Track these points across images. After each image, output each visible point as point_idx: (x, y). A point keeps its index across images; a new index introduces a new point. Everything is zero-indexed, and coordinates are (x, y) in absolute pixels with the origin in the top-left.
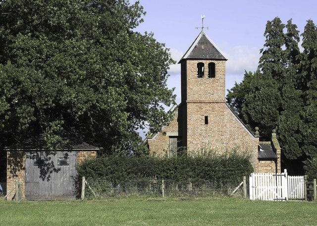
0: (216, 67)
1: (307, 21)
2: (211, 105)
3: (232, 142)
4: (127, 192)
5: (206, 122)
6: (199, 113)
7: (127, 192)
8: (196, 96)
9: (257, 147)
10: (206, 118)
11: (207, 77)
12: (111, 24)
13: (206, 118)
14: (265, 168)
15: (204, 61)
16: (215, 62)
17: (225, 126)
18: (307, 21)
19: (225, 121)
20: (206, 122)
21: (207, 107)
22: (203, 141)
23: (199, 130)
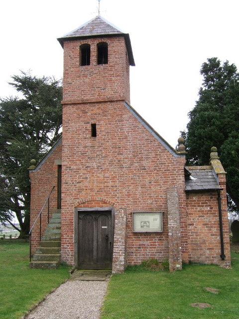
0: (109, 49)
1: (181, 132)
2: (102, 106)
3: (136, 164)
4: (37, 296)
5: (94, 134)
6: (82, 119)
7: (37, 296)
8: (77, 93)
9: (182, 172)
10: (94, 126)
11: (95, 64)
12: (11, 106)
13: (94, 126)
14: (199, 209)
15: (89, 42)
16: (108, 41)
17: (126, 138)
18: (181, 132)
19: (126, 130)
20: (94, 134)
21: (96, 109)
22: (88, 165)
23: (81, 148)
